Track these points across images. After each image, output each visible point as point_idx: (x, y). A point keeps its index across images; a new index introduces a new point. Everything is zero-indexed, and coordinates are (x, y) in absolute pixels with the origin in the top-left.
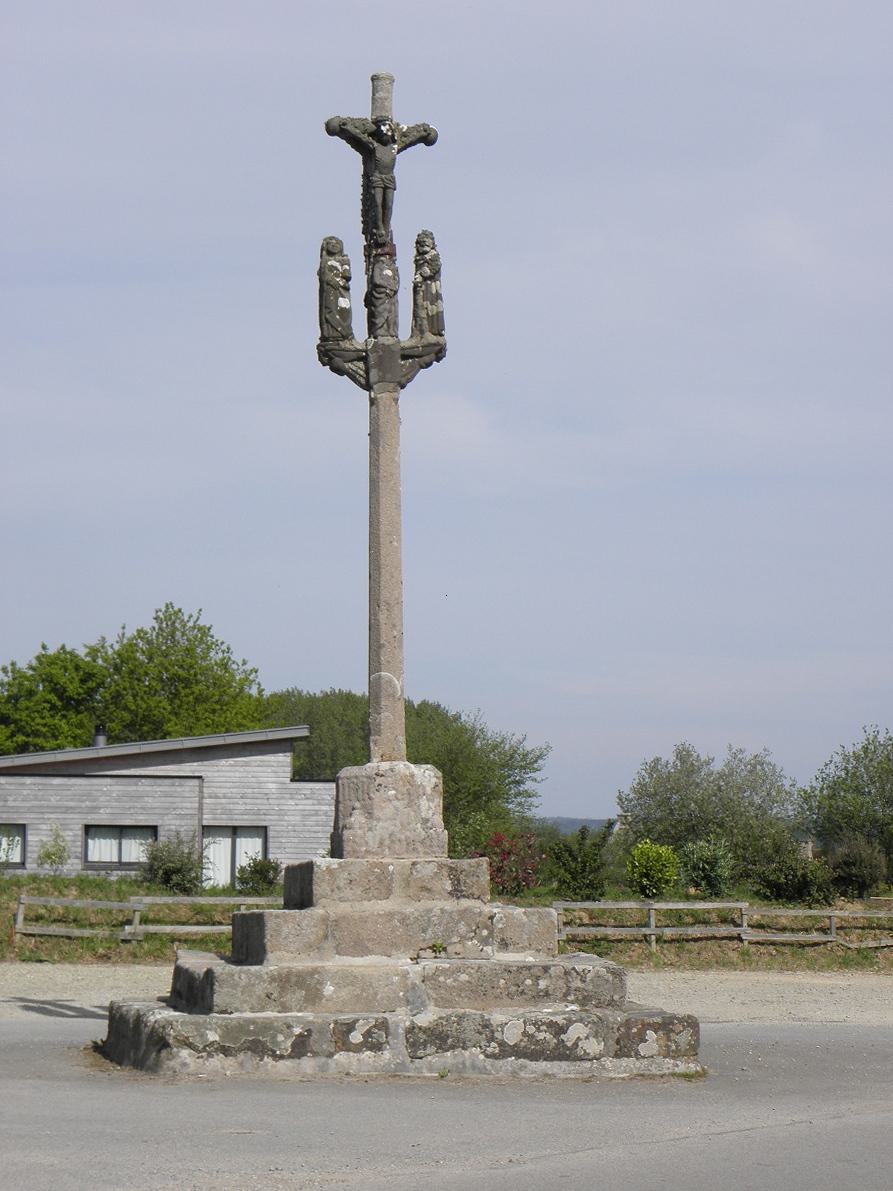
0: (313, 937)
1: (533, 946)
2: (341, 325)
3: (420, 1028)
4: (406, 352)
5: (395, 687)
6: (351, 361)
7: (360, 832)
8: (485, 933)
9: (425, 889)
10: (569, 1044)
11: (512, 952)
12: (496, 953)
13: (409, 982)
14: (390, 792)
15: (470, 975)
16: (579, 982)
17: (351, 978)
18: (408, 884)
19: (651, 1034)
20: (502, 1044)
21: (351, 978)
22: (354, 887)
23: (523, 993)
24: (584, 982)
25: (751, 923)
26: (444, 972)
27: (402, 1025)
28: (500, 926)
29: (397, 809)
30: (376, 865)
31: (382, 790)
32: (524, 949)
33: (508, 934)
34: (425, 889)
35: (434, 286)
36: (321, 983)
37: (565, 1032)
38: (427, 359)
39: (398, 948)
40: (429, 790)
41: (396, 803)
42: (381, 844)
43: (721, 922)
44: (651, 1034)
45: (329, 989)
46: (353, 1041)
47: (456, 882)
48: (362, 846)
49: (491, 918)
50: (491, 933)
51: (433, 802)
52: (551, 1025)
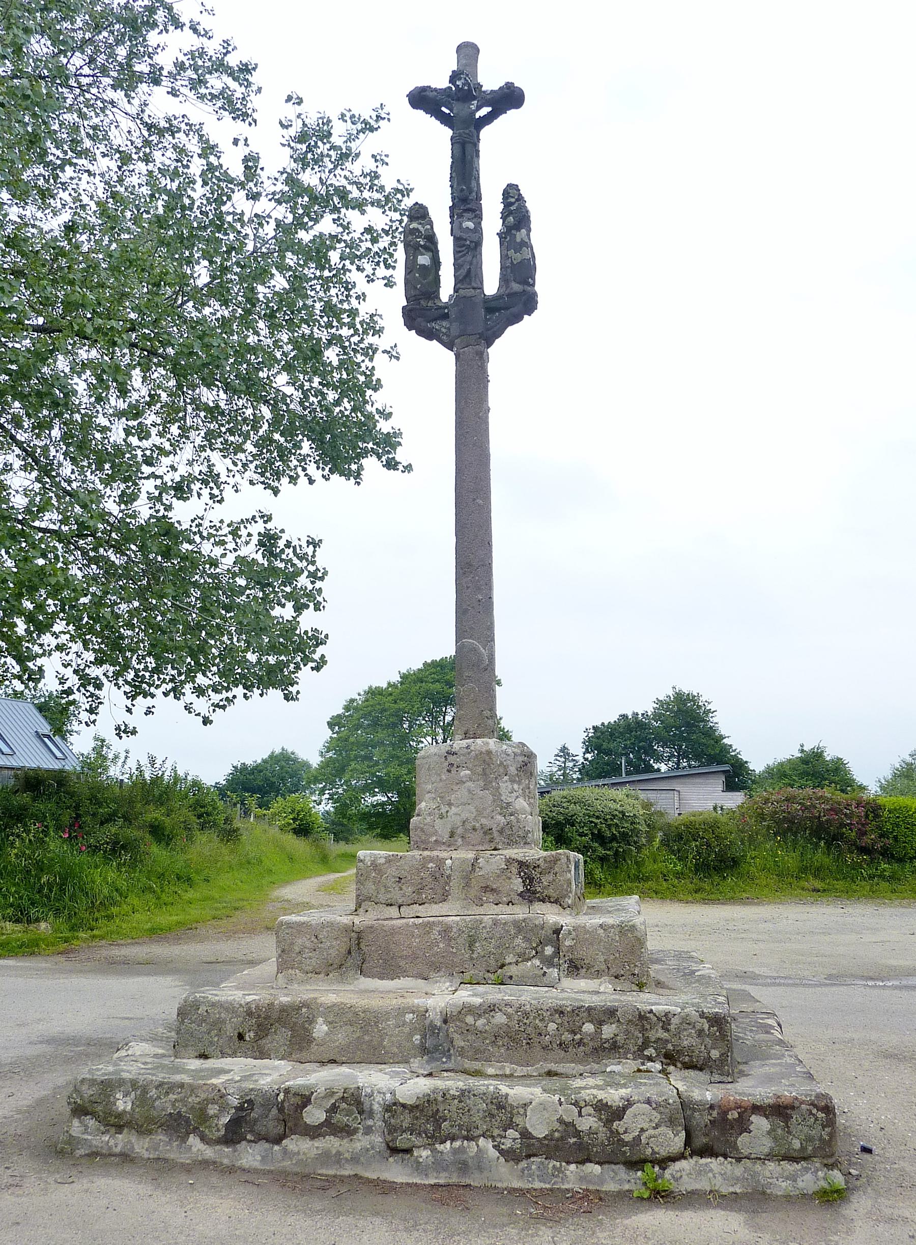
0: (333, 952)
1: (612, 971)
2: (420, 283)
3: (404, 1106)
4: (493, 304)
5: (480, 655)
6: (435, 320)
7: (428, 819)
8: (549, 950)
9: (487, 889)
10: (628, 1138)
11: (584, 978)
12: (563, 979)
13: (427, 1022)
14: (462, 773)
15: (509, 1016)
16: (660, 1031)
17: (350, 1015)
18: (468, 885)
19: (760, 1123)
20: (525, 1134)
21: (350, 1015)
22: (404, 887)
23: (580, 1043)
24: (668, 1030)
25: (391, 1144)
26: (467, 1009)
27: (379, 1098)
28: (567, 943)
29: (469, 791)
30: (431, 860)
31: (454, 770)
32: (598, 974)
33: (580, 953)
34: (487, 889)
35: (521, 235)
36: (311, 1021)
37: (620, 1118)
38: (514, 310)
39: (438, 969)
40: (513, 770)
41: (469, 784)
42: (452, 835)
43: (424, 1050)
44: (760, 1123)
45: (321, 1028)
46: (308, 1121)
47: (528, 880)
48: (432, 836)
49: (557, 931)
50: (557, 952)
51: (519, 783)
52: (601, 1107)
